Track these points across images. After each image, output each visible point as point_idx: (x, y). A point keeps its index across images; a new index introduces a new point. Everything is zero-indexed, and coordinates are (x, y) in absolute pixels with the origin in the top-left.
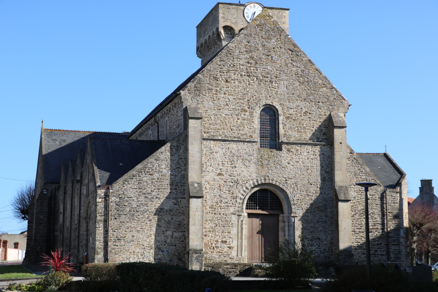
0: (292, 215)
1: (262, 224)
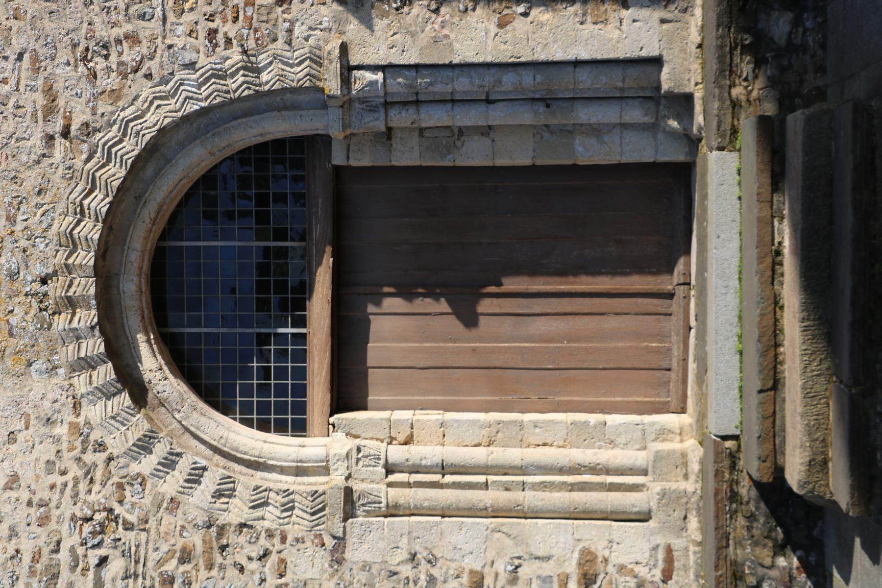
0: (332, 85)
1: (407, 292)
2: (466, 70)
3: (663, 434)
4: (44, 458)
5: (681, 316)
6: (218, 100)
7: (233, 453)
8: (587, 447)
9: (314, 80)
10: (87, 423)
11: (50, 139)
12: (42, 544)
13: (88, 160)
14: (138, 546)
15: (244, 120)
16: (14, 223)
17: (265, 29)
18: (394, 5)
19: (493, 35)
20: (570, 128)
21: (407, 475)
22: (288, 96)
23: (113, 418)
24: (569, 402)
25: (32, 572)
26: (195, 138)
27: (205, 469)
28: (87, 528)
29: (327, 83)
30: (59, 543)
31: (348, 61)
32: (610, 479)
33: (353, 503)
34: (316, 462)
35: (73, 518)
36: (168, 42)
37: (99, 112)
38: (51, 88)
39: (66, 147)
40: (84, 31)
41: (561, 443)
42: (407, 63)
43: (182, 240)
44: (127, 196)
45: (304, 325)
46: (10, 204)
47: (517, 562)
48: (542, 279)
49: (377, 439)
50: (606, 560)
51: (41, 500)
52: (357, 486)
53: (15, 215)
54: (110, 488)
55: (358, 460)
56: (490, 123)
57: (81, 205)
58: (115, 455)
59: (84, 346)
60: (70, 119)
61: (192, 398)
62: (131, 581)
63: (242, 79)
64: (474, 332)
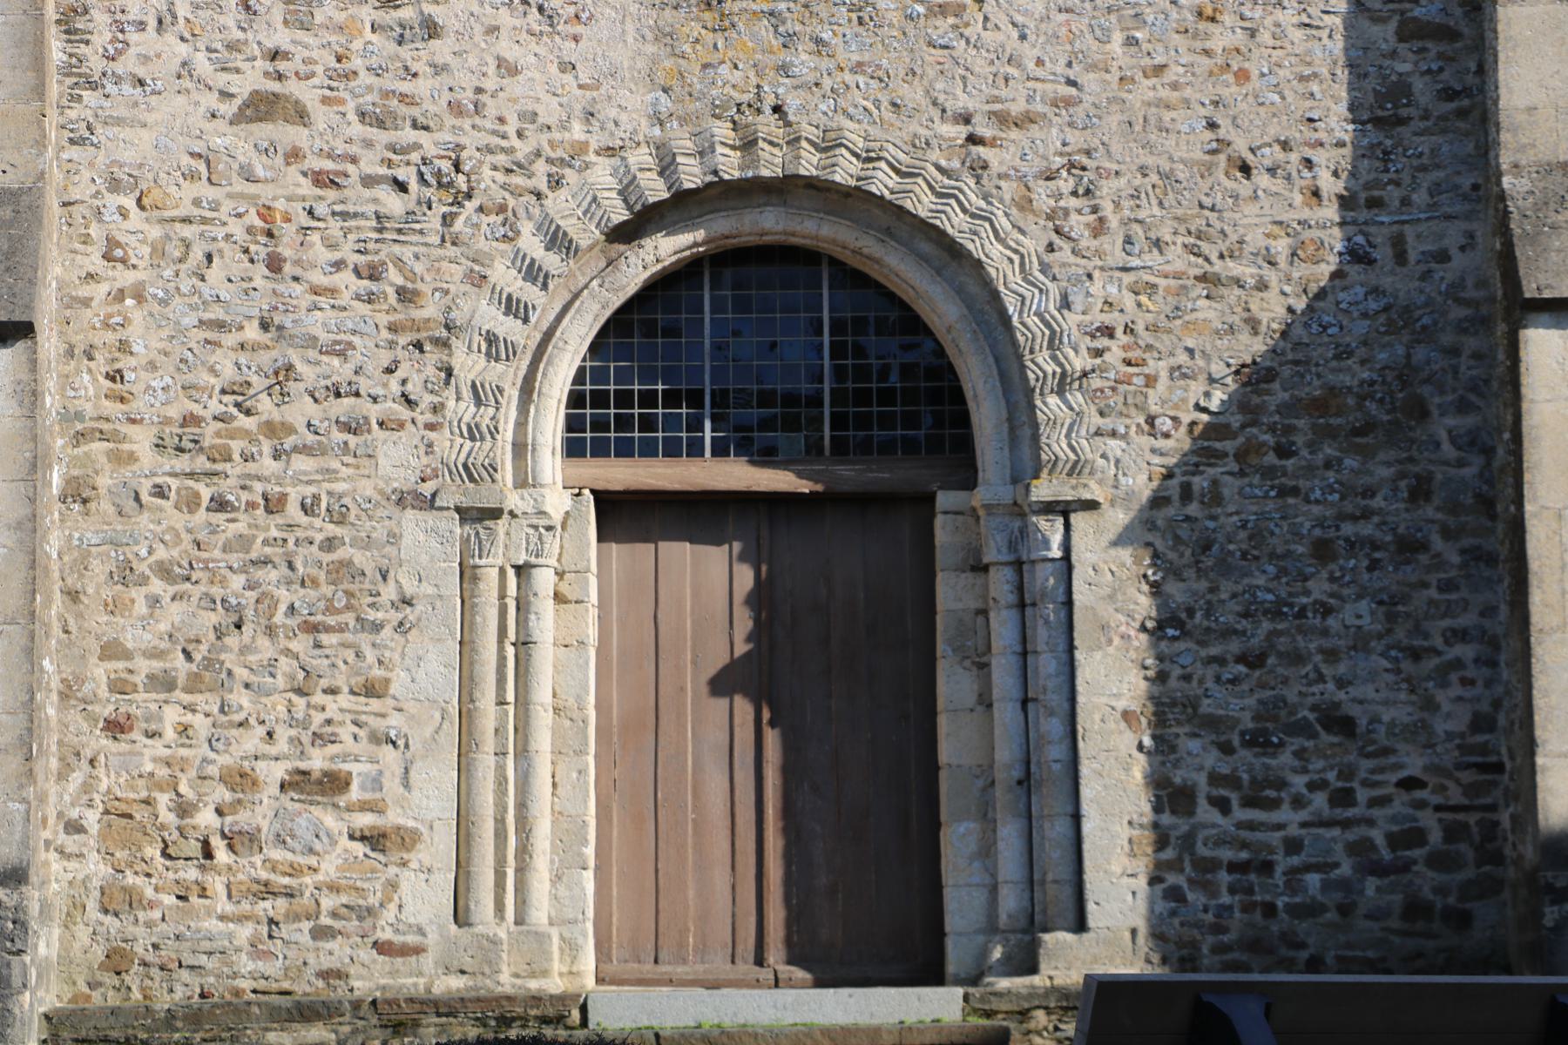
0: (1043, 490)
1: (760, 599)
2: (1067, 669)
3: (571, 949)
4: (540, 109)
5: (731, 976)
6: (1021, 339)
7: (545, 359)
8: (553, 844)
10: (587, 166)
11: (967, 120)
12: (425, 106)
13: (938, 168)
14: (421, 232)
15: (995, 372)
16: (853, 71)
17: (1115, 401)
18: (1150, 572)
19: (1114, 704)
20: (990, 815)
21: (515, 594)
22: (1027, 431)
23: (595, 199)
24: (610, 821)
25: (386, 94)
26: (969, 307)
27: (526, 320)
28: (446, 166)
29: (1046, 483)
30: (426, 128)
31: (1075, 511)
32: (510, 873)
33: (480, 520)
34: (533, 471)
35: (459, 147)
36: (1096, 274)
37: (1002, 184)
38: (1032, 121)
39: (955, 139)
40: (1107, 165)
41: (557, 808)
42: (1075, 589)
43: (831, 288)
44: (892, 219)
45: (714, 454)
46: (879, 67)
47: (401, 743)
48: (778, 782)
49: (560, 555)
50: (404, 864)
51: (484, 105)
52: (502, 525)
53: (864, 73)
54: (499, 195)
55: (536, 527)
56: (996, 705)
57: (879, 159)
58: (545, 202)
59: (691, 161)
60: (993, 145)
61: (617, 301)
62: (374, 224)
63: (1049, 370)
64: (705, 689)
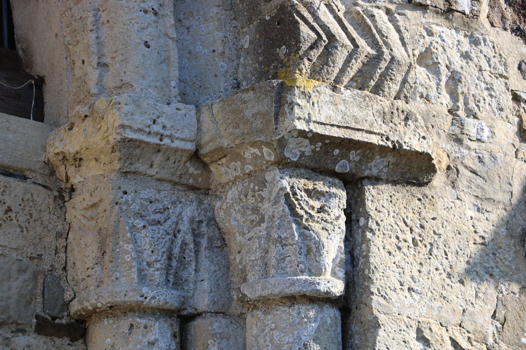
9: (315, 54)
31: (376, 180)
